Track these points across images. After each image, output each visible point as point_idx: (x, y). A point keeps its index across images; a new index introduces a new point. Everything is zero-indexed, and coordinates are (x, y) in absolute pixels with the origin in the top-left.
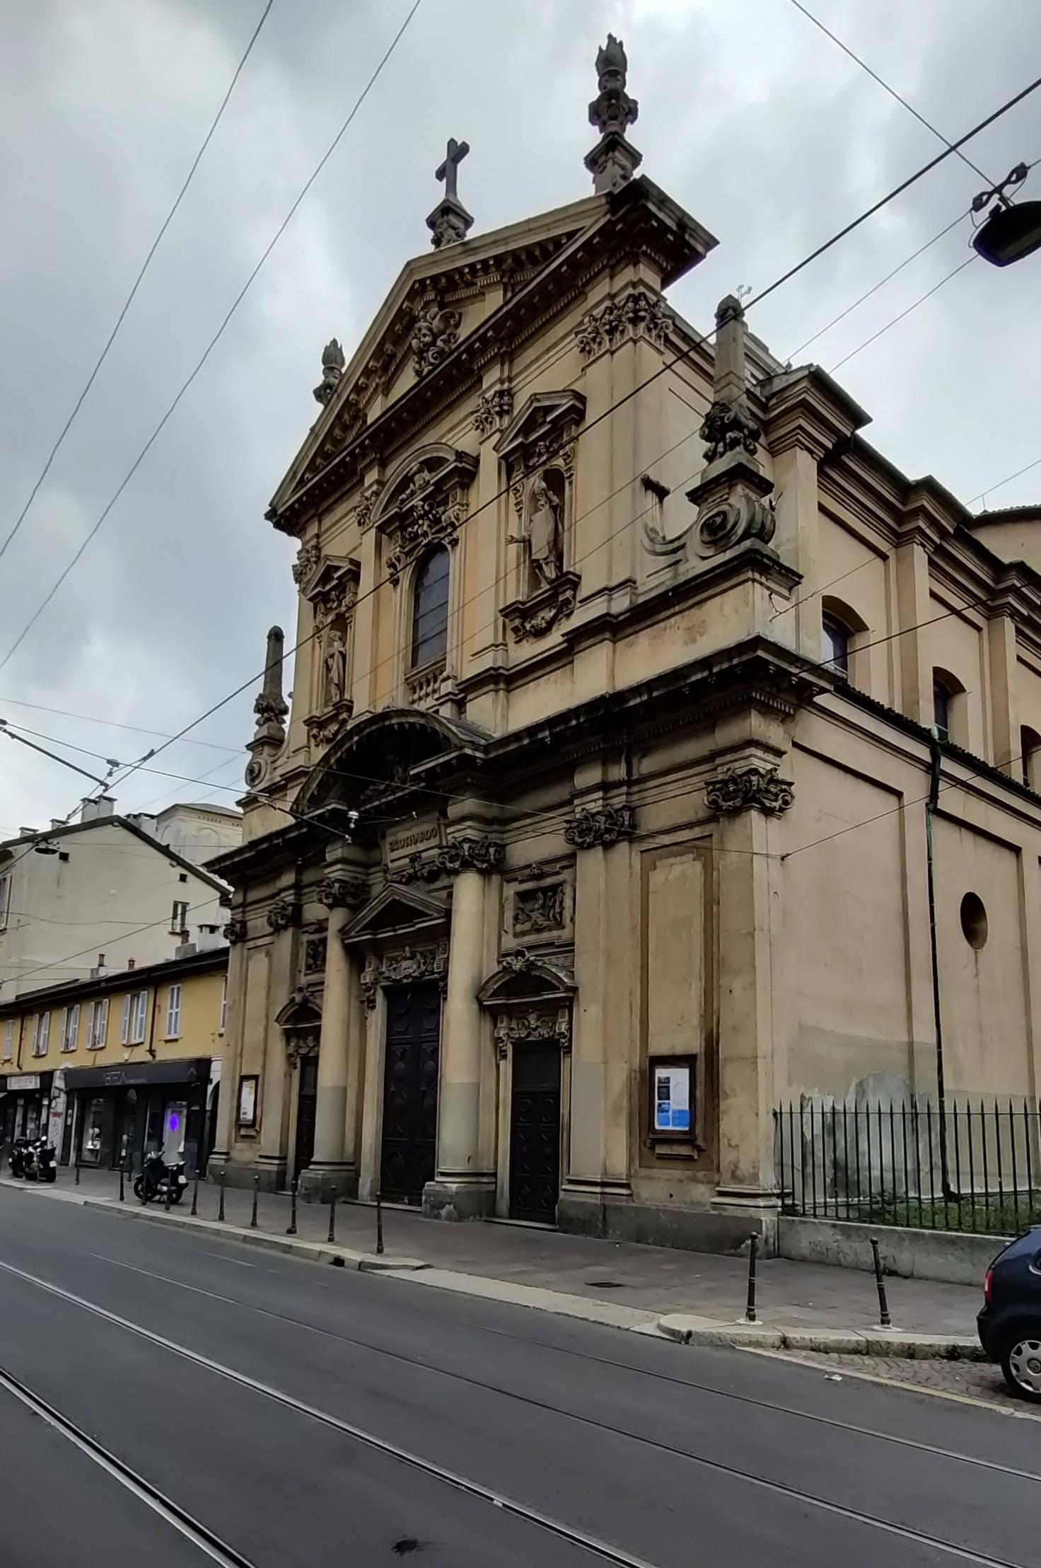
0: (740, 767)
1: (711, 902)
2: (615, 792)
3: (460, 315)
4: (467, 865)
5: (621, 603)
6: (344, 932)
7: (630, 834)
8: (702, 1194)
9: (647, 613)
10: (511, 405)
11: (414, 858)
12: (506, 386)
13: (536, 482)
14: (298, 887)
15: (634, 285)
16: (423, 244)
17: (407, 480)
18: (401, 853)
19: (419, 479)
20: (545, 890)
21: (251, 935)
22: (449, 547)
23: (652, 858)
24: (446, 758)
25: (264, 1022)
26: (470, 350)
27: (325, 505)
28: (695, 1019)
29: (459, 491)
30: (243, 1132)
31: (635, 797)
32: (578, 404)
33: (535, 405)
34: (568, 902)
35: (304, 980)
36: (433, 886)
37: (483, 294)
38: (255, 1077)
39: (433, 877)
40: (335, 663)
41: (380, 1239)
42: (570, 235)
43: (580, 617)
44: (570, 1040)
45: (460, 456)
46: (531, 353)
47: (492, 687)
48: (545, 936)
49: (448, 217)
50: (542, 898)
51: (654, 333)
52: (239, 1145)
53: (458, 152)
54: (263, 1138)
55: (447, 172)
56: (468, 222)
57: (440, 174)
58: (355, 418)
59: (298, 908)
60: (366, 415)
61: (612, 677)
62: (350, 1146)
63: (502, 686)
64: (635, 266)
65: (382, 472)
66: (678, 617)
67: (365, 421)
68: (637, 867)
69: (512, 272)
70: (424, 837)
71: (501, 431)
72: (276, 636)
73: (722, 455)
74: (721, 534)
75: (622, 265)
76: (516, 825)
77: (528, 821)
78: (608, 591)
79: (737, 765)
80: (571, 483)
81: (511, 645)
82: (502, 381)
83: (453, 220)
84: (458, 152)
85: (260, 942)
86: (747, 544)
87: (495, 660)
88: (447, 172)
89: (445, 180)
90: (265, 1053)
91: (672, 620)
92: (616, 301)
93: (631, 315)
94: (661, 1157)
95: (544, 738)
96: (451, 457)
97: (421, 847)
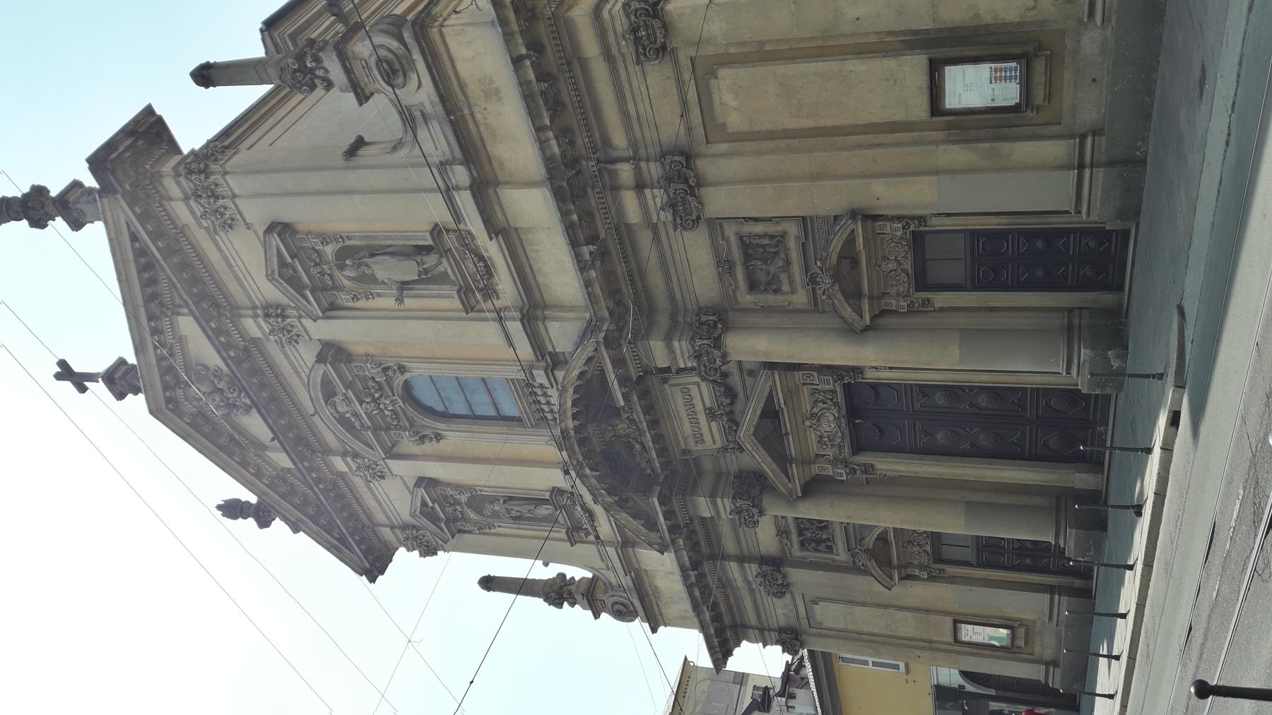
0: (621, 24)
1: (761, 54)
2: (646, 174)
3: (197, 365)
4: (718, 343)
5: (461, 175)
6: (791, 500)
7: (688, 156)
8: (1091, 42)
9: (470, 148)
10: (278, 306)
11: (711, 414)
12: (259, 312)
13: (345, 278)
14: (741, 559)
15: (177, 175)
16: (136, 403)
17: (342, 420)
18: (705, 430)
19: (342, 408)
20: (747, 258)
21: (793, 622)
22: (407, 376)
23: (714, 129)
24: (608, 361)
25: (891, 611)
26: (228, 346)
27: (363, 517)
28: (890, 63)
29: (353, 364)
30: (1021, 643)
31: (651, 151)
32: (278, 229)
33: (276, 276)
34: (759, 228)
35: (842, 556)
36: (741, 395)
37: (180, 337)
38: (955, 622)
39: (731, 393)
40: (516, 508)
41: (1147, 376)
42: (134, 238)
43: (474, 224)
44: (913, 218)
45: (320, 358)
46: (232, 286)
47: (540, 323)
48: (795, 255)
49: (120, 380)
50: (755, 256)
51: (219, 156)
52: (1037, 650)
53: (65, 372)
54: (1029, 616)
55: (80, 381)
56: (122, 362)
57: (82, 389)
58: (284, 480)
59: (764, 560)
60: (283, 469)
61: (531, 184)
62: (1037, 500)
63: (539, 313)
64: (162, 176)
65: (336, 453)
66: (476, 110)
67: (289, 470)
68: (724, 147)
69: (162, 305)
70: (689, 404)
71: (300, 317)
72: (489, 583)
73: (327, 71)
74: (397, 66)
75: (160, 188)
76: (677, 290)
77: (675, 280)
78: (448, 193)
79: (619, 30)
80: (349, 238)
81: (498, 304)
82: (255, 316)
83: (117, 376)
84: (65, 372)
85: (802, 612)
86: (407, 36)
87: (514, 319)
88: (80, 381)
89: (86, 384)
90: (928, 611)
91: (479, 116)
92: (189, 192)
93: (202, 176)
94: (1049, 97)
95: (591, 253)
96: (321, 369)
97: (699, 408)
